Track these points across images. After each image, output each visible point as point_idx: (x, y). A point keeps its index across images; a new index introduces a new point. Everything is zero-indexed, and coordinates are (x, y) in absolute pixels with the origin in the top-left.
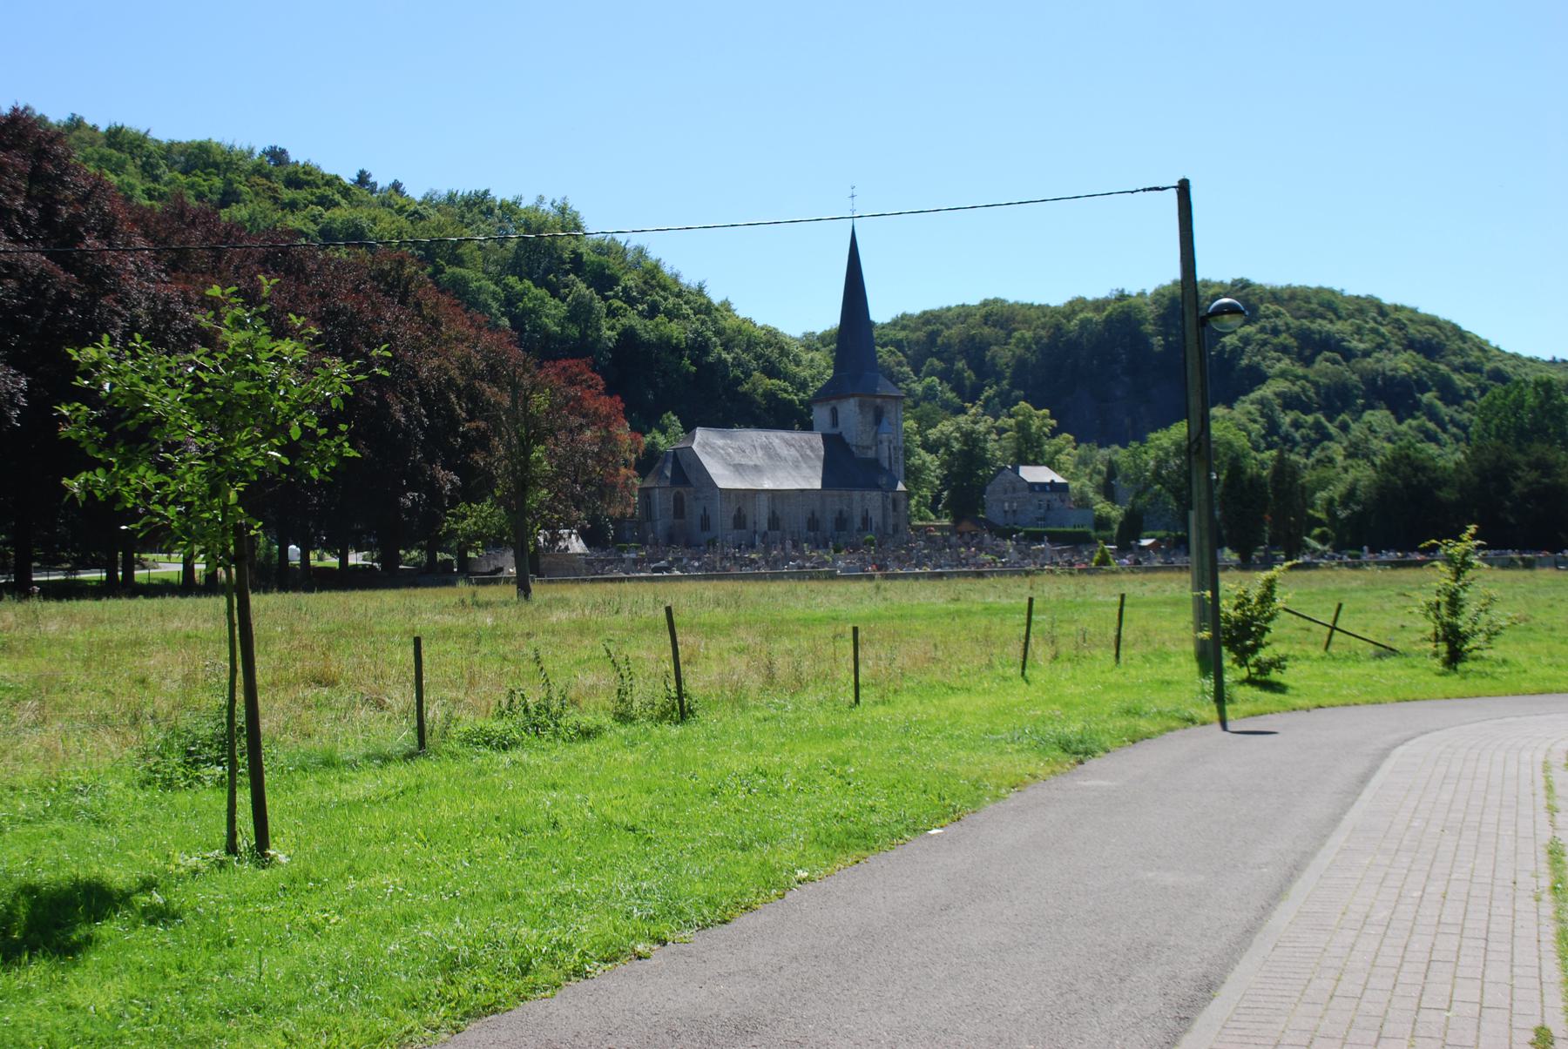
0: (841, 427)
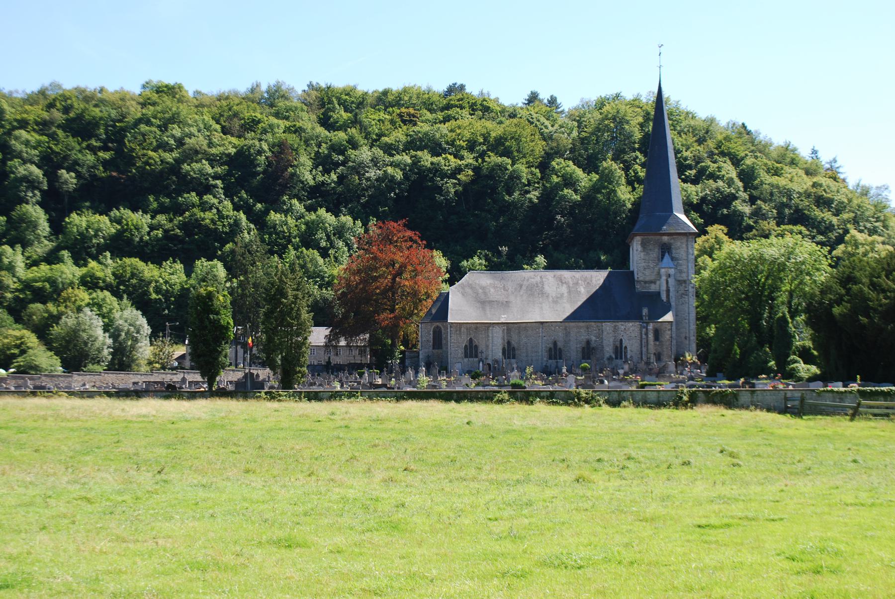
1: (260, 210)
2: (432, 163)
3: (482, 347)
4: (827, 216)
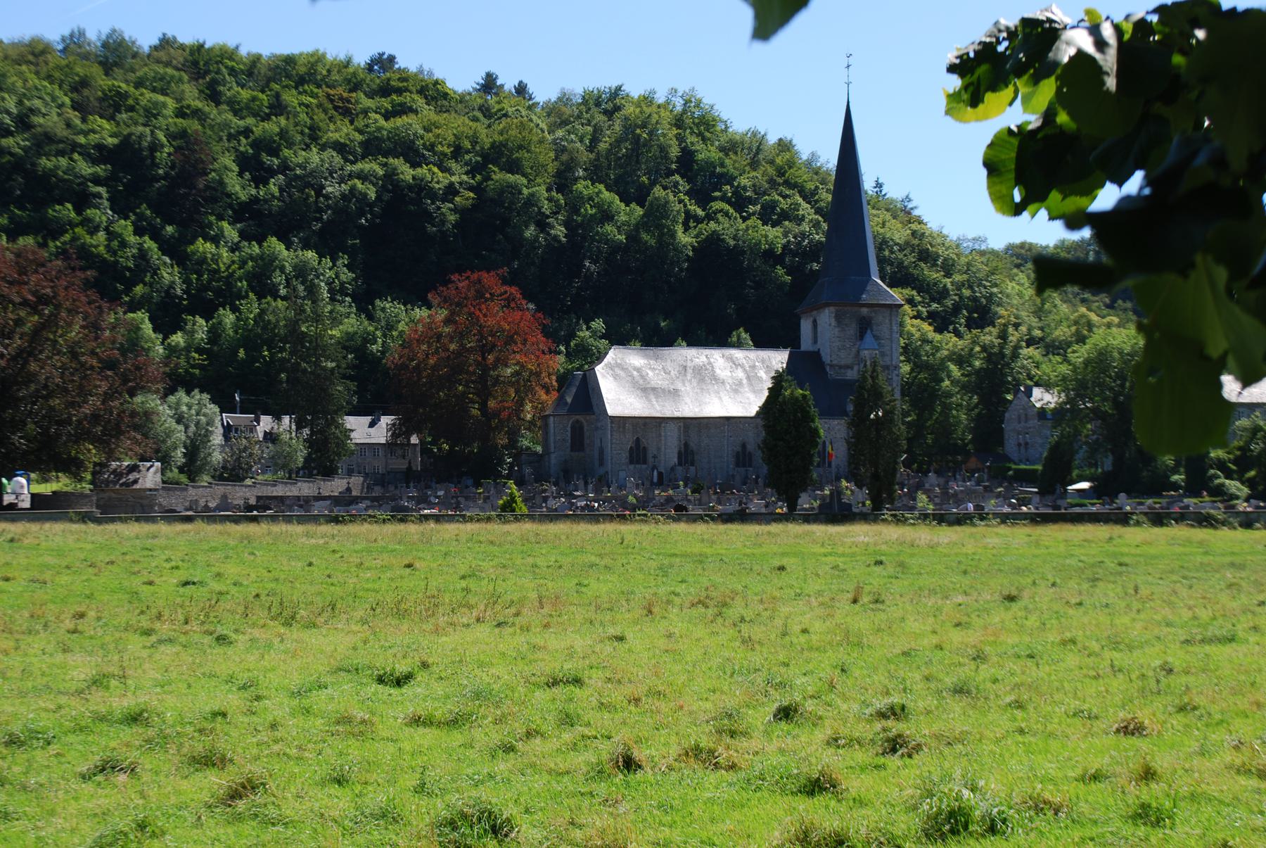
0: (819, 346)
1: (172, 236)
2: (414, 178)
3: (652, 451)
4: (935, 275)
